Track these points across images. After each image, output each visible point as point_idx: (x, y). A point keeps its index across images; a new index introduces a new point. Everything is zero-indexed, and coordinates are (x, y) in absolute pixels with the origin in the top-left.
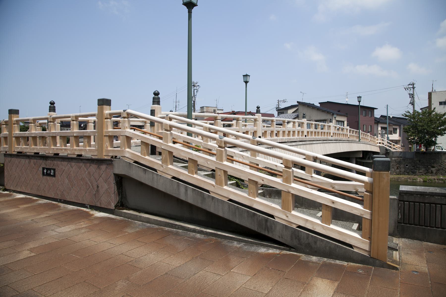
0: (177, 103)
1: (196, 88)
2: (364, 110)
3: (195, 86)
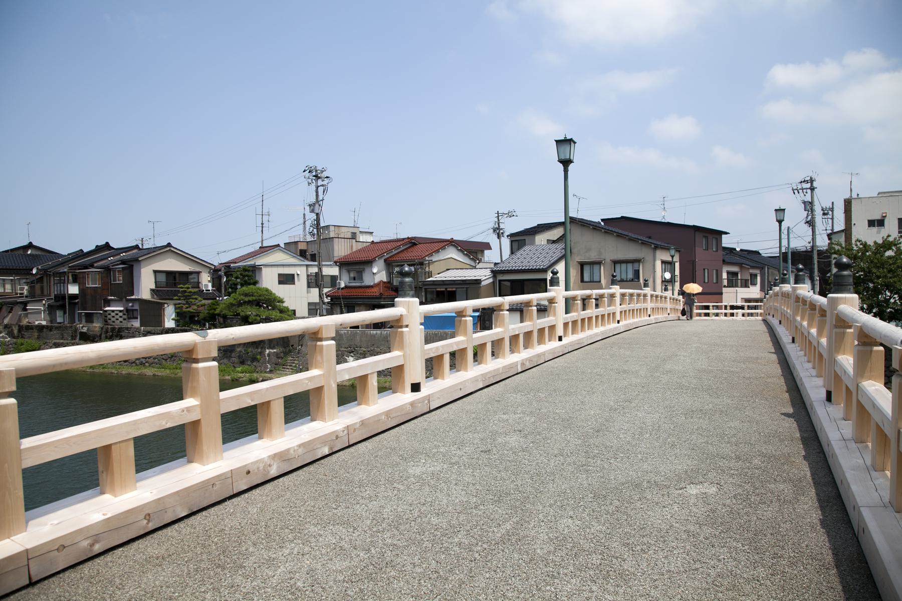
0: (265, 218)
2: (705, 237)
3: (319, 178)
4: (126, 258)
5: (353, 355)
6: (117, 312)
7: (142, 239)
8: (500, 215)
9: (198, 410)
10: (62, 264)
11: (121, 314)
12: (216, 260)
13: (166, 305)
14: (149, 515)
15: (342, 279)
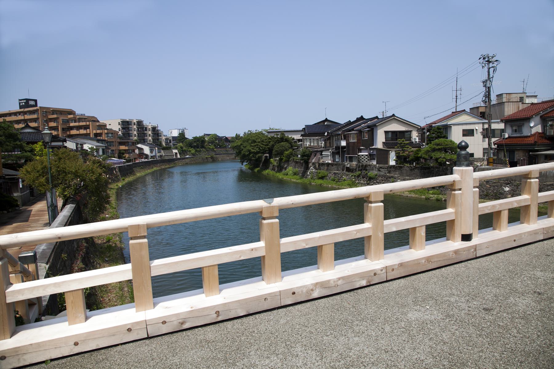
0: (459, 92)
1: (493, 65)
4: (370, 124)
5: (509, 186)
6: (365, 156)
7: (383, 112)
9: (264, 250)
10: (339, 129)
11: (366, 157)
12: (423, 124)
13: (390, 152)
14: (218, 312)
15: (506, 132)
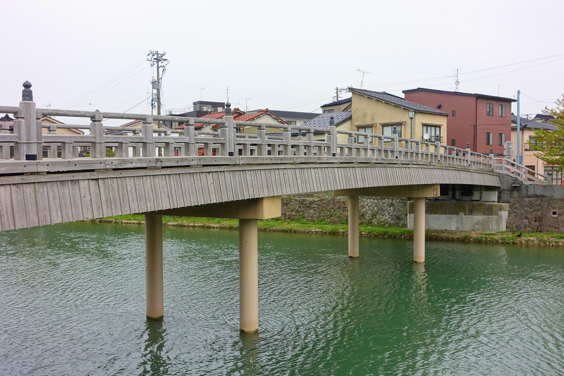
1: (162, 65)
8: (338, 90)
